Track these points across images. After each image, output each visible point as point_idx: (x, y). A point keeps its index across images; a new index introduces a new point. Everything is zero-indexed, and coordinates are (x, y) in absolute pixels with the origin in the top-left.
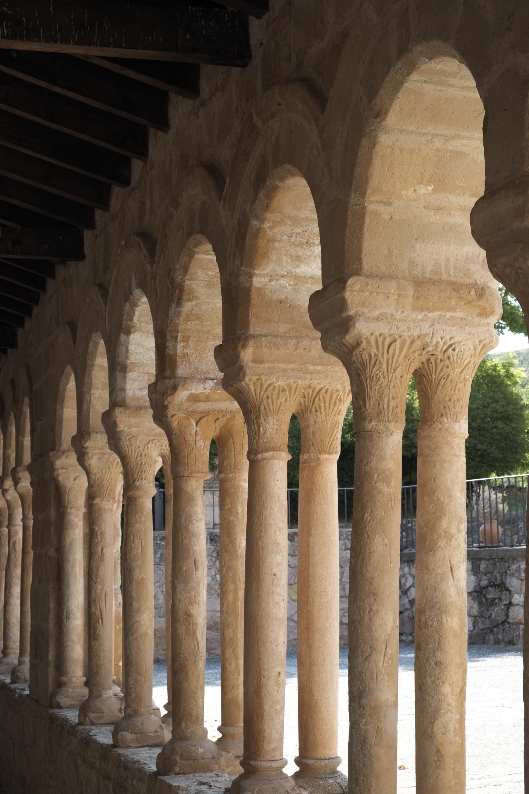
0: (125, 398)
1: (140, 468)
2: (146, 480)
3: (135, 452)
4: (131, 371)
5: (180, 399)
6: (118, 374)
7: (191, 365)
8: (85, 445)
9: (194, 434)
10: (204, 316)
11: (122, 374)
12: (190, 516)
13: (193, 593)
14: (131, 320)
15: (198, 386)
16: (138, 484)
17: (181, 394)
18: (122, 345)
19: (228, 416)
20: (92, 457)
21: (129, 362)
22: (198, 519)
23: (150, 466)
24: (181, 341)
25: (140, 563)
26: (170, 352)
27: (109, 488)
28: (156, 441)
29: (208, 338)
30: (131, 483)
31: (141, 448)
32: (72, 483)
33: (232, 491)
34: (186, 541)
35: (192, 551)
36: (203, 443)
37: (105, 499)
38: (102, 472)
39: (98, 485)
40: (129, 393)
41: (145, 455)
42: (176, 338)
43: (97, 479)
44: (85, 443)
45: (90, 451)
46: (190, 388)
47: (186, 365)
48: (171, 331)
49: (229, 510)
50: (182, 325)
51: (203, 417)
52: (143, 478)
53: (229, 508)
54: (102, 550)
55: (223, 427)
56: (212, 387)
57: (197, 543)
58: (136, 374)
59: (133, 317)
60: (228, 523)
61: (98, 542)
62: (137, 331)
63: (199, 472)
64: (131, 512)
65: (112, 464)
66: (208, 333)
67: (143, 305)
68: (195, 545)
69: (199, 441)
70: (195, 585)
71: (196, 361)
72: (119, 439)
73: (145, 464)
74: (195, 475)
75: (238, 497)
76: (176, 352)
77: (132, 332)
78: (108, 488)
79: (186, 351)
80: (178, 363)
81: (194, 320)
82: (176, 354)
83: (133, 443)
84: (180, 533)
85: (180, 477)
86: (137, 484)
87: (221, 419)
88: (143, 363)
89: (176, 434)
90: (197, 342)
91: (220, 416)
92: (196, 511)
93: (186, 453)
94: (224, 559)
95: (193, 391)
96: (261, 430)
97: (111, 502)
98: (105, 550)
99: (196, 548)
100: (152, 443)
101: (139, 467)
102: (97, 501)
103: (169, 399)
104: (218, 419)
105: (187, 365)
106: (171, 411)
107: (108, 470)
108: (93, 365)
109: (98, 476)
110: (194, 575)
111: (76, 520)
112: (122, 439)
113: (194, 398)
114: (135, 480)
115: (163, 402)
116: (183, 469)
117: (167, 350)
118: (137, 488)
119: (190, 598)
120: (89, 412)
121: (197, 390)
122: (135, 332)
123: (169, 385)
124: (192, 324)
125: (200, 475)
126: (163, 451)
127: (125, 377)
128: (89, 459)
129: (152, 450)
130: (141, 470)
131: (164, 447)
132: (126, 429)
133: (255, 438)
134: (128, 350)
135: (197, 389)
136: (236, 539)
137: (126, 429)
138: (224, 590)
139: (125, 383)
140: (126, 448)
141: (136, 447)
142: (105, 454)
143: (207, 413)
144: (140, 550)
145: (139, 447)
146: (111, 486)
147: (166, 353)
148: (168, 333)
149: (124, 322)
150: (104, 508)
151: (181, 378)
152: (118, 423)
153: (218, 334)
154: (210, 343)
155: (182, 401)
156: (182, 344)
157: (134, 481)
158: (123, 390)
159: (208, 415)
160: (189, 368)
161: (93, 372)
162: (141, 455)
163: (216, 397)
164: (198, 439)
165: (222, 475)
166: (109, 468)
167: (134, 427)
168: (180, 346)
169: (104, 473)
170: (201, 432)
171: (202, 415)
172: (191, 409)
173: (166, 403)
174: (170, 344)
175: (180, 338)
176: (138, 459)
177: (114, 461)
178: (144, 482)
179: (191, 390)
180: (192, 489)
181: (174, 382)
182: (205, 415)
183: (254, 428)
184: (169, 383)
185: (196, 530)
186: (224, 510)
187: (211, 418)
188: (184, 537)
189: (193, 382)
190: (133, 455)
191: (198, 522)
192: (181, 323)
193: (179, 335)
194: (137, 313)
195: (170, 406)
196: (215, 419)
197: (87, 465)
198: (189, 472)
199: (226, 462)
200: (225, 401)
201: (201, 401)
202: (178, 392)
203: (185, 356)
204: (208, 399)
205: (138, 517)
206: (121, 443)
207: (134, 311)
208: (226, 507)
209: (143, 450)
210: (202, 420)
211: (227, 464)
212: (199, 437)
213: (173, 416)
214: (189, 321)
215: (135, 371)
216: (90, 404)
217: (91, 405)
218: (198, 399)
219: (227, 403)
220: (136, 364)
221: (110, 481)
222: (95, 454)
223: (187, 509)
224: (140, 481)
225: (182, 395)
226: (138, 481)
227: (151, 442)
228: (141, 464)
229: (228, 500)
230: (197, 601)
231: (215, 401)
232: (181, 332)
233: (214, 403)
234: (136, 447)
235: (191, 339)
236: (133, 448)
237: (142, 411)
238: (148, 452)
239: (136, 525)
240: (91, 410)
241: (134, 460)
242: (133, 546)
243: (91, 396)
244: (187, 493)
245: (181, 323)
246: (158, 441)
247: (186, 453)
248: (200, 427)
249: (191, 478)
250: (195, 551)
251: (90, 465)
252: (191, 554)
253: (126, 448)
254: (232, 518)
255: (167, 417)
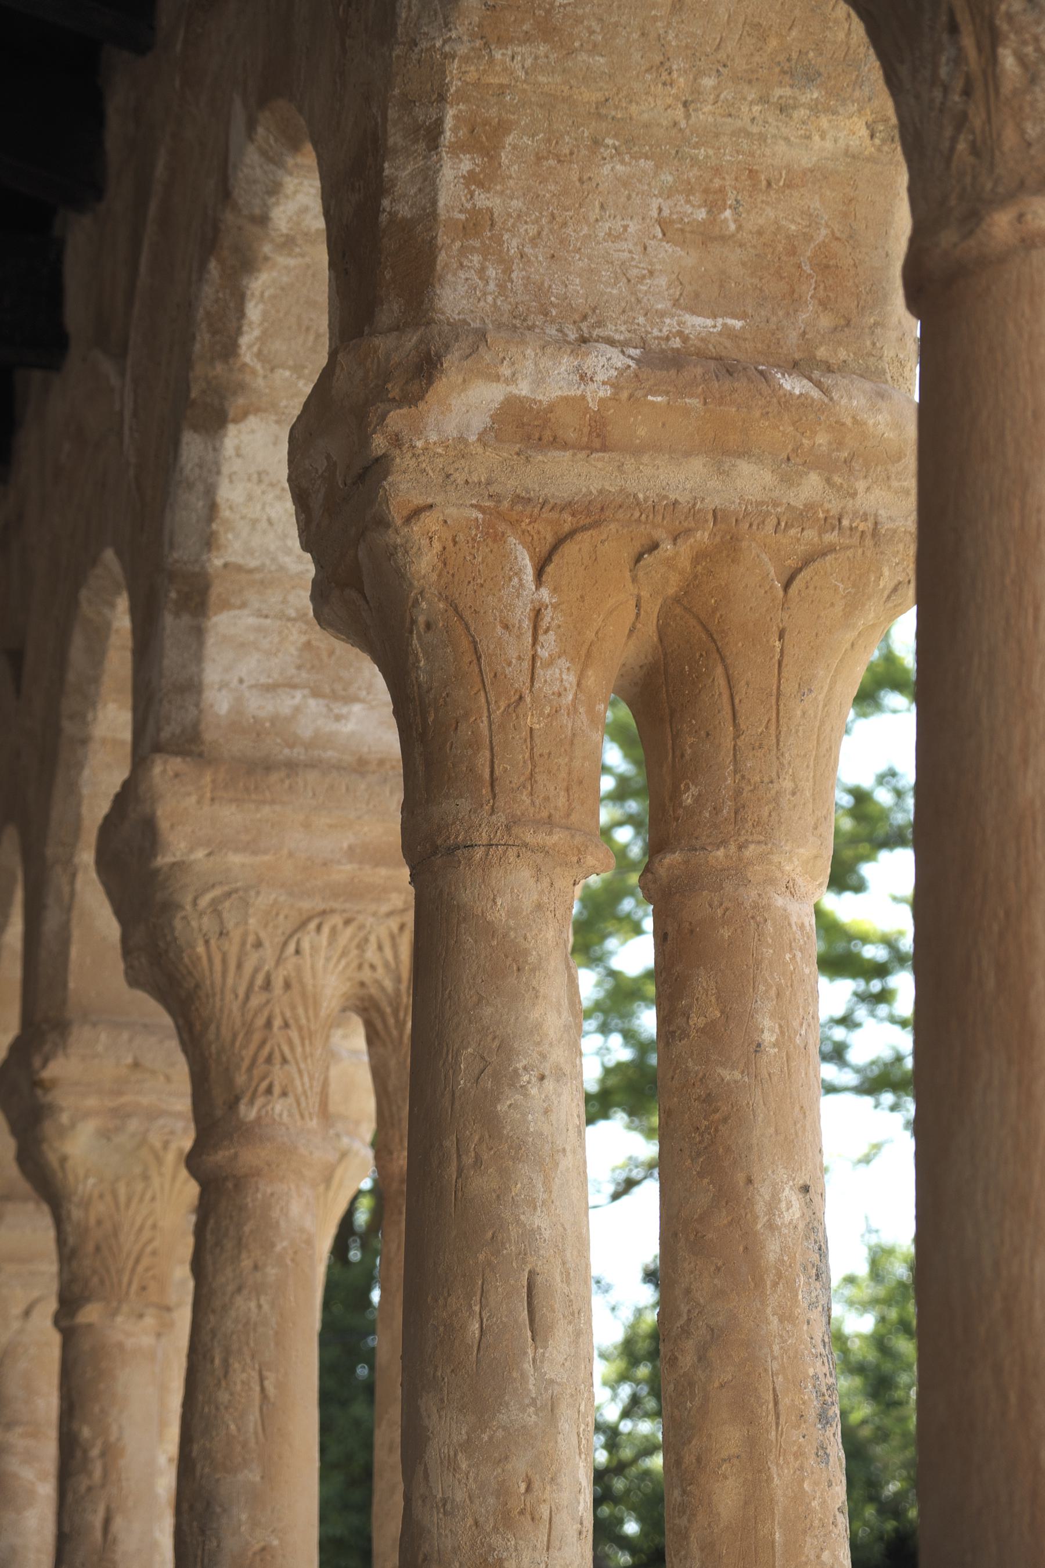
0: (196, 725)
1: (263, 1043)
2: (291, 1100)
3: (239, 966)
4: (225, 605)
5: (451, 430)
6: (170, 623)
7: (508, 271)
8: (46, 1074)
9: (527, 624)
10: (579, 20)
11: (186, 619)
12: (506, 1049)
13: (519, 1465)
14: (229, 350)
15: (545, 362)
16: (253, 1114)
17: (457, 402)
18: (190, 486)
19: (703, 536)
20: (73, 1125)
21: (218, 562)
22: (547, 1068)
23: (307, 1036)
24: (458, 148)
25: (253, 1475)
26: (404, 211)
27: (145, 1262)
28: (337, 920)
29: (597, 143)
30: (219, 1113)
31: (269, 952)
32: (16, 1325)
33: (726, 933)
34: (482, 1183)
35: (514, 1232)
36: (570, 679)
37: (125, 1308)
38: (114, 1194)
39: (98, 1249)
40: (219, 702)
41: (287, 986)
42: (432, 134)
43: (92, 1221)
44: (45, 1064)
45: (66, 1102)
46: (505, 371)
47: (483, 269)
48: (407, 103)
49: (709, 1030)
50: (466, 59)
51: (572, 534)
52: (277, 1090)
53: (713, 1023)
54: (107, 1522)
55: (677, 600)
56: (621, 372)
57: (541, 1195)
58: (252, 621)
59: (239, 331)
60: (708, 1099)
61: (90, 1489)
62: (258, 410)
63: (549, 823)
64: (218, 1244)
65: (159, 1161)
66: (600, 117)
67: (282, 260)
68: (533, 1204)
69: (550, 663)
70: (531, 1418)
71: (538, 255)
72: (170, 907)
73: (286, 1025)
74: (529, 838)
75: (758, 963)
76: (434, 202)
77: (231, 414)
78: (137, 1261)
79: (483, 200)
80: (442, 257)
81: (528, 38)
82: (433, 214)
83: (230, 925)
84: (450, 1143)
85: (451, 850)
86: (248, 1112)
87: (667, 547)
88: (282, 568)
89: (428, 626)
90: (539, 159)
91: (660, 534)
92: (538, 1026)
93: (484, 726)
94: (688, 1291)
95: (523, 389)
96: (1008, 61)
97: (149, 1321)
98: (118, 1523)
99: (539, 1220)
100: (319, 928)
101: (257, 1037)
102: (90, 1314)
103: (397, 419)
104: (654, 546)
105: (491, 272)
106: (403, 487)
107: (139, 1186)
108: (85, 741)
109: (99, 1208)
110: (528, 1367)
111: (27, 1474)
112: (180, 907)
113: (526, 428)
114: (237, 1099)
115: (365, 441)
116: (465, 805)
117: (386, 203)
118: (248, 1133)
119: (503, 1491)
120: (65, 942)
121: (539, 380)
122: (245, 415)
123: (395, 358)
124: (517, 61)
125: (557, 837)
126: (366, 975)
127: (199, 633)
128: (63, 1132)
129: (321, 963)
130: (265, 1052)
131: (371, 954)
132: (200, 854)
133: (962, 121)
134: (212, 508)
135: (543, 377)
136: (750, 1181)
137: (200, 854)
138: (689, 1459)
139: (198, 658)
140: (201, 949)
141: (243, 943)
142: (129, 1115)
143: (589, 515)
144: (253, 1417)
145: (258, 944)
146: (154, 1253)
147: (384, 218)
148: (392, 114)
149: (199, 369)
150: (120, 1346)
151: (458, 329)
152: (164, 825)
153: (647, 126)
154: (606, 170)
155: (462, 439)
156: (466, 165)
157: (233, 1104)
158: (192, 687)
159: (596, 524)
160: (502, 286)
161: (86, 773)
162: (267, 985)
163: (642, 432)
164: (543, 653)
165: (672, 859)
166: (146, 1177)
167: (237, 850)
168: (453, 171)
169: (122, 1198)
170: (559, 619)
171: (568, 521)
172: (510, 484)
173: (379, 443)
174: (400, 171)
175: (455, 130)
176: (255, 1001)
177: (166, 1145)
178: (279, 1107)
179: (513, 379)
180: (514, 912)
181: (421, 341)
182: (584, 521)
183: (959, 59)
184: (394, 347)
185: (535, 1123)
186: (685, 1034)
187: (613, 544)
188: (468, 1160)
189: (523, 342)
190: (230, 981)
191: (549, 1084)
192: (462, 50)
193: (450, 113)
194: (254, 312)
195: (403, 461)
196: (637, 546)
197: (53, 1158)
198: (500, 818)
199: (694, 790)
200: (687, 454)
201: (565, 446)
202: (441, 386)
203: (476, 223)
204: (597, 436)
205: (246, 1263)
206: (178, 924)
207: (240, 298)
208: (697, 1021)
209: (279, 961)
210: (570, 549)
211: (697, 799)
212: (549, 644)
213: (417, 512)
214: (502, 41)
215: (244, 605)
216: (69, 909)
217: (75, 914)
218: (548, 435)
219: (698, 465)
220: (251, 571)
221: (146, 1234)
222: (87, 1115)
223: (488, 1011)
224: (260, 1101)
225: (464, 405)
226: (251, 1102)
227: (312, 925)
228: (269, 1024)
229: (703, 982)
230: (544, 1511)
231: (637, 451)
232: (462, 97)
233: (630, 464)
234: (243, 943)
235: (510, 139)
236: (233, 951)
237: (274, 777)
238: (298, 969)
239: (239, 1300)
240: (76, 933)
241: (235, 1007)
242: (223, 1397)
243: (74, 876)
244: (489, 930)
245: (462, 50)
246: (347, 922)
247: (484, 726)
248: (555, 590)
249: (512, 853)
250: (531, 1235)
251: (64, 1159)
252: (511, 1249)
253: (201, 949)
254: (727, 1075)
255: (383, 523)
